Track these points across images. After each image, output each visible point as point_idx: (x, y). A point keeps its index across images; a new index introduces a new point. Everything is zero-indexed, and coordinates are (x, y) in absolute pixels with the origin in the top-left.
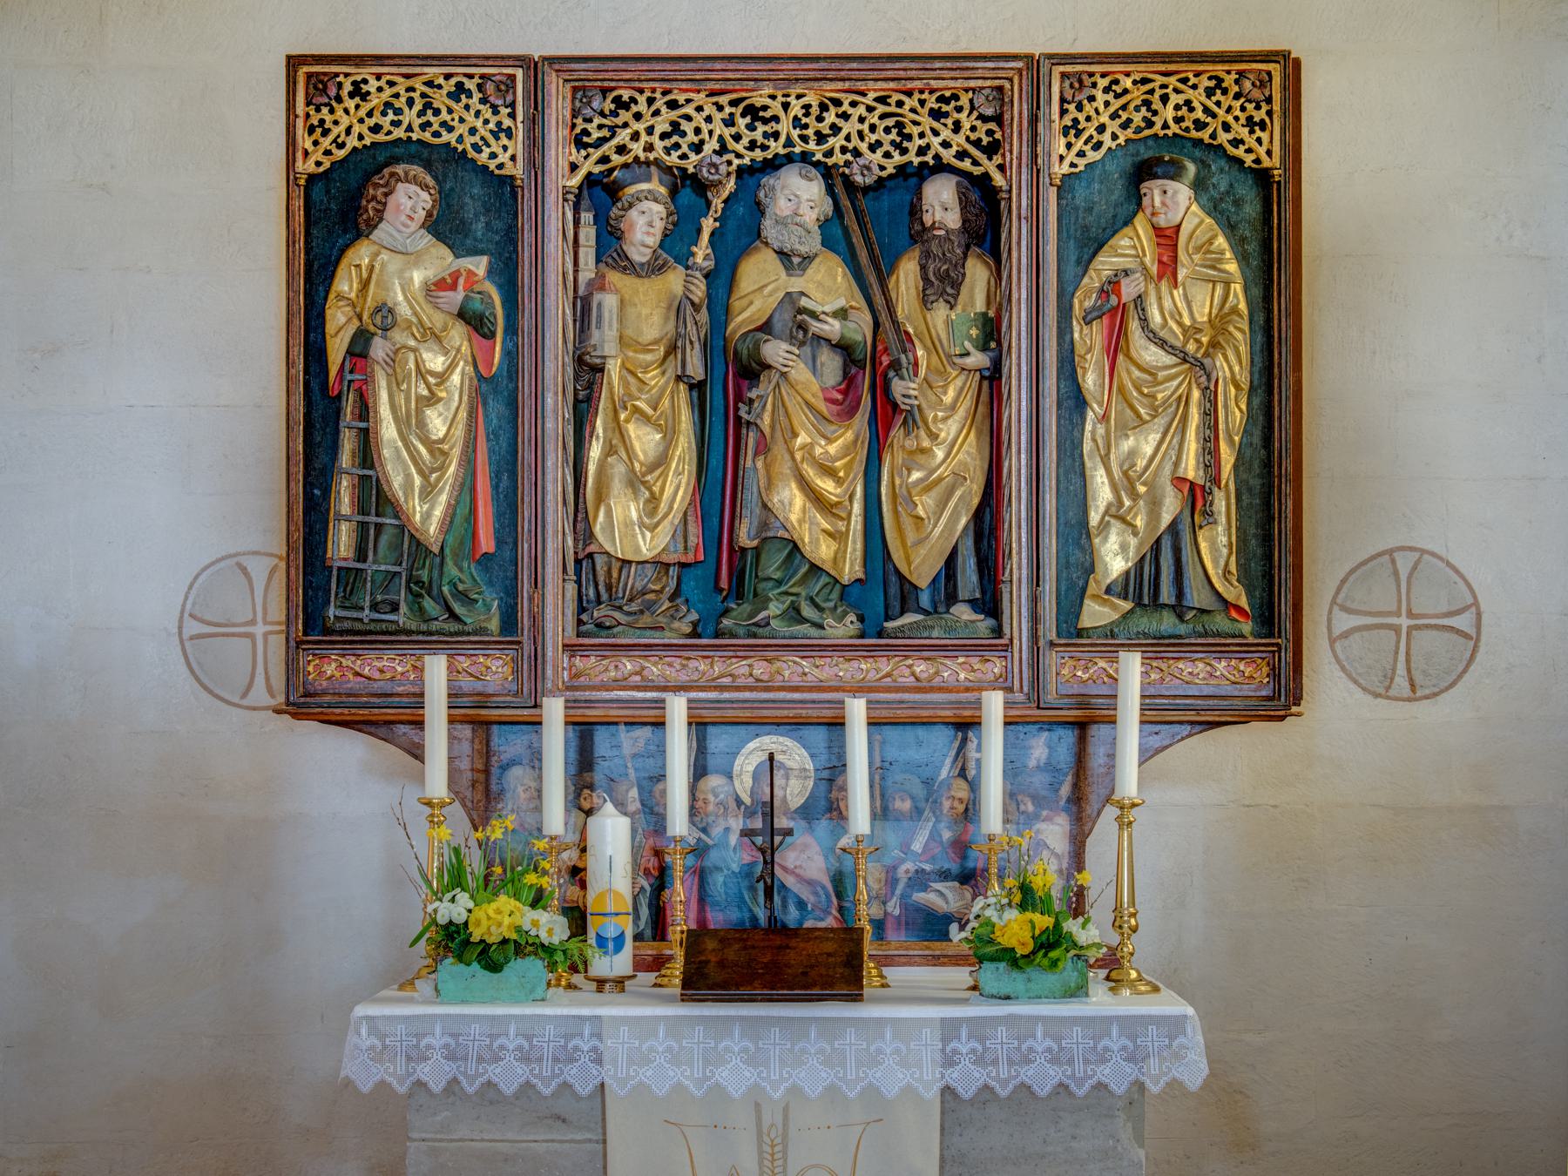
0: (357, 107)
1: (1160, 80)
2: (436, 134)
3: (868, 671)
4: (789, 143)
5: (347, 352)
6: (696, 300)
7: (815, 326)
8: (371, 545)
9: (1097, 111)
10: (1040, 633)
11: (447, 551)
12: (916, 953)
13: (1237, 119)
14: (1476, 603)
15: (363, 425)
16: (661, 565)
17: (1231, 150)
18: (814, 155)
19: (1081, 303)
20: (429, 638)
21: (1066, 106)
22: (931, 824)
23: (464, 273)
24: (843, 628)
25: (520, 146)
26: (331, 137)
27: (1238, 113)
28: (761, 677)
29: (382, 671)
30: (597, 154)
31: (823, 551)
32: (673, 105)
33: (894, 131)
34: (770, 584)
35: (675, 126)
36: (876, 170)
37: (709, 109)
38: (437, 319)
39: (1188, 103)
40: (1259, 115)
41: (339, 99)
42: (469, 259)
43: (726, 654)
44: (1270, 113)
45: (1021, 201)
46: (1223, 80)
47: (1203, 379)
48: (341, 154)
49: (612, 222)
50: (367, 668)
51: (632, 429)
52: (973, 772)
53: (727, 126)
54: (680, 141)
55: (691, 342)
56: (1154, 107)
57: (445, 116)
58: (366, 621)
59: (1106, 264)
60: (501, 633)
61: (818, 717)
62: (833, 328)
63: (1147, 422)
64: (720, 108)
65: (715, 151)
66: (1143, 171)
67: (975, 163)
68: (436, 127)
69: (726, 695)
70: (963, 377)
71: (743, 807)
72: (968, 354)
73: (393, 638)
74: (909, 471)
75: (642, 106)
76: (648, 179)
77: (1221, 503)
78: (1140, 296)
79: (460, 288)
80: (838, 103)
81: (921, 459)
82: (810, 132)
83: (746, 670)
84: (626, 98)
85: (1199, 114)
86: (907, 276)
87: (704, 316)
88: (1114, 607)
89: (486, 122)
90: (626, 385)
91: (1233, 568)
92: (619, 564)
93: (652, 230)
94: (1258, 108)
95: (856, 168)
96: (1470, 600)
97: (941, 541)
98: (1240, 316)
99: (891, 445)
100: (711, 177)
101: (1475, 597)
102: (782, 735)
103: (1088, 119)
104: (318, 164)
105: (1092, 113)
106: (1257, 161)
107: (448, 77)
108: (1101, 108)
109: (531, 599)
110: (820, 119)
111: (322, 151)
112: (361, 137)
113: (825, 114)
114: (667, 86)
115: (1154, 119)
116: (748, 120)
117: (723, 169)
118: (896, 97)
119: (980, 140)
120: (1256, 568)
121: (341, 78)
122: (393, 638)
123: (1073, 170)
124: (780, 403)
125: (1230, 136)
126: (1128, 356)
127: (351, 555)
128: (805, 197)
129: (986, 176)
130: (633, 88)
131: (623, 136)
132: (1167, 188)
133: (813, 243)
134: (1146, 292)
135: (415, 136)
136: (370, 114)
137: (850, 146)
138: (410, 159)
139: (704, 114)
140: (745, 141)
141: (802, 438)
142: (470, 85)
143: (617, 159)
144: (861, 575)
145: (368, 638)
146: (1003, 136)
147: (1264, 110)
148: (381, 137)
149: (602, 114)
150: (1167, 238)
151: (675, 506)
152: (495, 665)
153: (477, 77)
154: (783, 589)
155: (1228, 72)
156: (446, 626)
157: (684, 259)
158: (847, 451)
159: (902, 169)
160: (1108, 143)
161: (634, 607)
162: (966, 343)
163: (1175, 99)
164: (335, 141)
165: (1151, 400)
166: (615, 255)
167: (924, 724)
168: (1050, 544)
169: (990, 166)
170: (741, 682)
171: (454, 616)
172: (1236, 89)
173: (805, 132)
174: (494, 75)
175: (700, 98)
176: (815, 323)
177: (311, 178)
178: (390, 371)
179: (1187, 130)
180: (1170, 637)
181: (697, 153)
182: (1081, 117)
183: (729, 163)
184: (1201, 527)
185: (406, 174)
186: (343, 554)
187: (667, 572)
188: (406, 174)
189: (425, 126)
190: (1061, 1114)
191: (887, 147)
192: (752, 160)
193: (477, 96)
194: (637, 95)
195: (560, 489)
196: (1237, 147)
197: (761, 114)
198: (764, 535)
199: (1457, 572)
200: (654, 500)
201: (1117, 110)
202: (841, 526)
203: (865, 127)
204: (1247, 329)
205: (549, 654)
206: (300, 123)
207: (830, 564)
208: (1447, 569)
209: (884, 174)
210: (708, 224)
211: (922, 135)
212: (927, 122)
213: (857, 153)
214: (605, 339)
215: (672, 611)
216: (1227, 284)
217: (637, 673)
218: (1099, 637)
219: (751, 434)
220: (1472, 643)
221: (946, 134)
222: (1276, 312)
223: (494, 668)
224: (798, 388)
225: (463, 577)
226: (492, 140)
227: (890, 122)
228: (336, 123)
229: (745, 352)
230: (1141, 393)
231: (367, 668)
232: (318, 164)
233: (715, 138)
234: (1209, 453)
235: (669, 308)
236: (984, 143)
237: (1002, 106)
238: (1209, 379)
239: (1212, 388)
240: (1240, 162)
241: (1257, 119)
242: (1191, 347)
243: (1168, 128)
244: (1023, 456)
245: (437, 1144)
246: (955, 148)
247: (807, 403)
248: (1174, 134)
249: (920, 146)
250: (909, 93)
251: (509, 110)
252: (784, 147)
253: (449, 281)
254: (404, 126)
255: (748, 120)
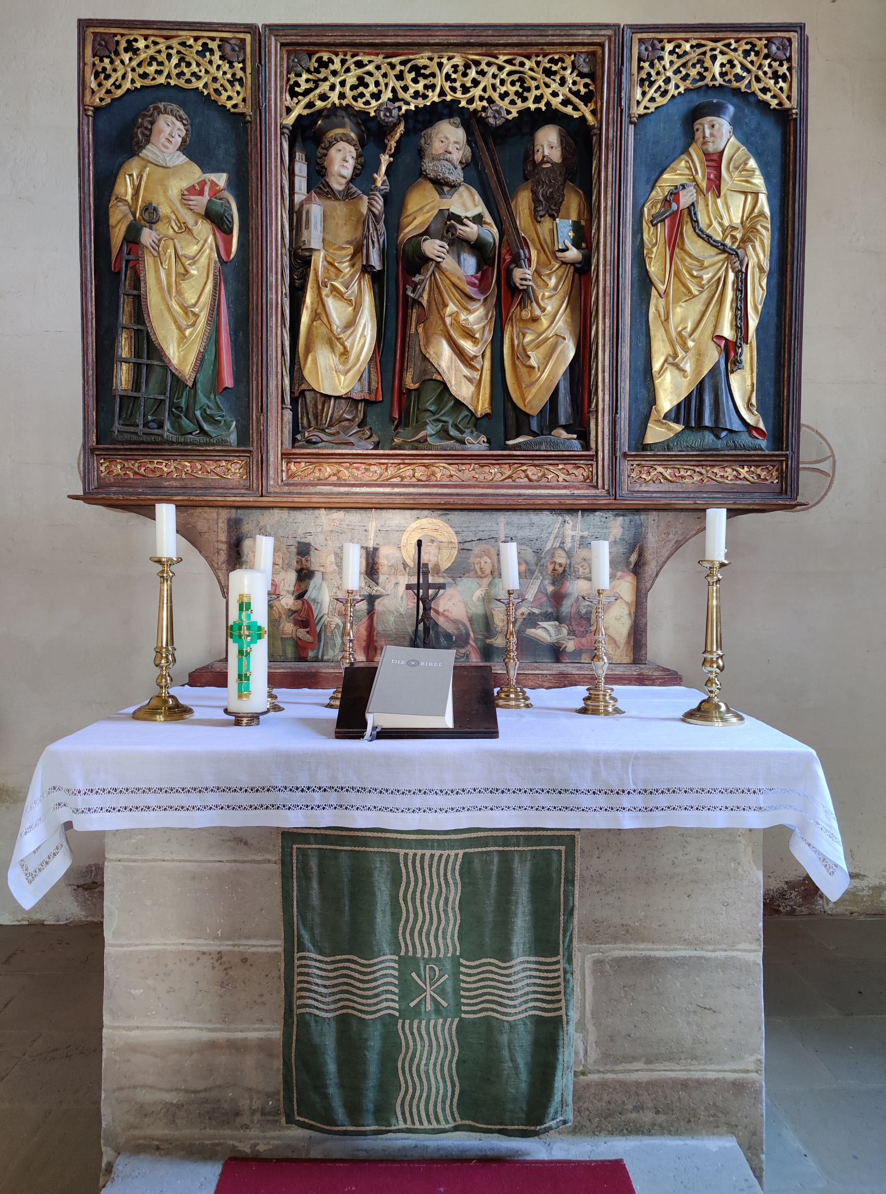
0: (131, 59)
1: (711, 45)
2: (188, 81)
3: (495, 474)
4: (442, 93)
5: (124, 238)
6: (376, 212)
7: (461, 230)
8: (144, 380)
9: (665, 69)
10: (618, 447)
11: (199, 385)
12: (530, 672)
13: (765, 73)
14: (833, 456)
15: (135, 292)
16: (348, 398)
17: (761, 96)
18: (460, 102)
19: (649, 210)
20: (186, 447)
21: (642, 64)
22: (539, 581)
23: (209, 183)
24: (477, 444)
25: (249, 91)
26: (111, 81)
27: (766, 69)
28: (421, 478)
29: (153, 471)
30: (305, 101)
31: (462, 390)
32: (360, 64)
33: (518, 84)
34: (428, 414)
35: (361, 79)
36: (504, 113)
37: (385, 68)
38: (189, 218)
39: (730, 62)
40: (784, 70)
41: (117, 53)
42: (213, 175)
43: (396, 461)
44: (790, 69)
45: (607, 134)
46: (755, 46)
47: (737, 264)
48: (119, 93)
49: (318, 160)
50: (143, 469)
51: (331, 303)
52: (569, 545)
53: (398, 80)
54: (365, 91)
55: (373, 242)
56: (706, 65)
57: (194, 68)
58: (140, 434)
59: (670, 179)
60: (238, 445)
61: (462, 504)
62: (471, 231)
63: (695, 296)
64: (393, 66)
65: (389, 99)
66: (695, 114)
67: (576, 109)
68: (188, 76)
69: (397, 490)
70: (562, 269)
71: (408, 569)
72: (567, 249)
73: (160, 447)
74: (524, 335)
75: (337, 66)
76: (343, 126)
77: (748, 354)
78: (693, 204)
79: (206, 193)
80: (477, 63)
81: (533, 326)
82: (457, 85)
83: (410, 473)
84: (325, 59)
85: (738, 70)
86: (523, 202)
87: (382, 226)
88: (670, 429)
89: (225, 73)
90: (326, 270)
91: (754, 401)
92: (322, 400)
93: (346, 164)
94: (781, 65)
95: (490, 113)
96: (829, 454)
97: (547, 382)
98: (766, 217)
99: (511, 319)
100: (387, 119)
101: (832, 452)
102: (435, 518)
103: (658, 73)
104: (101, 100)
105: (661, 69)
106: (780, 104)
107: (196, 39)
108: (668, 66)
109: (258, 420)
110: (465, 75)
111: (104, 91)
112: (133, 81)
113: (468, 71)
114: (355, 50)
115: (705, 74)
116: (413, 75)
117: (395, 112)
118: (519, 59)
119: (579, 91)
120: (770, 403)
121: (118, 38)
122: (160, 447)
123: (646, 111)
124: (435, 287)
125: (761, 86)
126: (683, 249)
127: (130, 387)
128: (452, 139)
129: (583, 118)
130: (330, 52)
131: (324, 87)
132: (715, 123)
133: (457, 176)
134: (697, 201)
135: (172, 83)
136: (140, 65)
137: (486, 96)
138: (171, 100)
139: (383, 71)
140: (411, 91)
141: (451, 308)
142: (213, 45)
143: (319, 104)
144: (489, 411)
145: (142, 446)
146: (596, 88)
147: (785, 66)
148: (148, 82)
149: (309, 71)
150: (714, 161)
151: (362, 358)
152: (234, 468)
153: (218, 40)
154: (436, 417)
155: (760, 39)
156: (197, 439)
157: (369, 189)
158: (480, 320)
159: (523, 113)
160: (672, 91)
161: (333, 430)
162: (566, 241)
163: (721, 59)
164: (114, 84)
165: (698, 280)
166: (321, 186)
167: (535, 510)
168: (625, 385)
169: (586, 111)
170: (406, 481)
171: (203, 432)
172: (766, 51)
173: (454, 85)
174: (231, 39)
175: (379, 60)
176: (459, 226)
177: (97, 109)
178: (156, 254)
179: (730, 81)
180: (710, 450)
181: (377, 101)
182: (653, 73)
183: (400, 108)
184: (732, 372)
185: (165, 109)
186: (124, 386)
187: (357, 407)
188: (165, 109)
189: (180, 75)
190: (688, 839)
191: (512, 96)
192: (416, 107)
193: (218, 54)
194: (334, 57)
195: (279, 342)
196: (765, 94)
197: (422, 71)
198: (423, 378)
199: (822, 437)
200: (345, 353)
201: (679, 67)
202: (476, 375)
203: (497, 82)
204: (769, 226)
205: (272, 459)
206: (88, 69)
207: (469, 401)
208: (817, 436)
209: (510, 117)
210: (385, 159)
211: (537, 88)
212: (540, 76)
213: (490, 101)
214: (314, 237)
215: (360, 434)
216: (756, 194)
217: (334, 475)
218: (659, 450)
219: (414, 311)
220: (830, 479)
221: (554, 86)
222: (790, 215)
223: (233, 470)
224: (447, 274)
225: (211, 405)
226: (228, 86)
227: (515, 77)
228: (115, 70)
229: (411, 249)
230: (692, 276)
231: (143, 469)
232: (101, 100)
233: (390, 89)
234: (740, 319)
235: (358, 221)
236: (582, 93)
237: (595, 66)
238: (741, 264)
239: (744, 270)
240: (768, 105)
241: (780, 73)
242: (728, 242)
243: (716, 80)
244: (607, 321)
245: (132, 864)
246: (561, 97)
247: (454, 285)
248: (720, 85)
249: (536, 96)
250: (529, 57)
251: (241, 65)
252: (439, 96)
253: (198, 188)
254: (165, 74)
255: (413, 75)
